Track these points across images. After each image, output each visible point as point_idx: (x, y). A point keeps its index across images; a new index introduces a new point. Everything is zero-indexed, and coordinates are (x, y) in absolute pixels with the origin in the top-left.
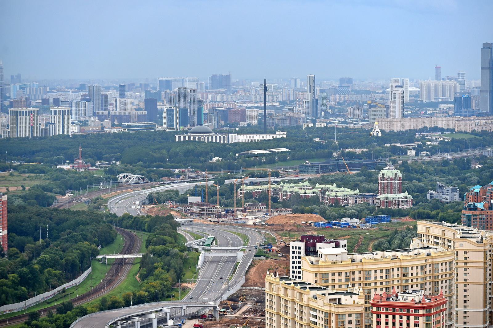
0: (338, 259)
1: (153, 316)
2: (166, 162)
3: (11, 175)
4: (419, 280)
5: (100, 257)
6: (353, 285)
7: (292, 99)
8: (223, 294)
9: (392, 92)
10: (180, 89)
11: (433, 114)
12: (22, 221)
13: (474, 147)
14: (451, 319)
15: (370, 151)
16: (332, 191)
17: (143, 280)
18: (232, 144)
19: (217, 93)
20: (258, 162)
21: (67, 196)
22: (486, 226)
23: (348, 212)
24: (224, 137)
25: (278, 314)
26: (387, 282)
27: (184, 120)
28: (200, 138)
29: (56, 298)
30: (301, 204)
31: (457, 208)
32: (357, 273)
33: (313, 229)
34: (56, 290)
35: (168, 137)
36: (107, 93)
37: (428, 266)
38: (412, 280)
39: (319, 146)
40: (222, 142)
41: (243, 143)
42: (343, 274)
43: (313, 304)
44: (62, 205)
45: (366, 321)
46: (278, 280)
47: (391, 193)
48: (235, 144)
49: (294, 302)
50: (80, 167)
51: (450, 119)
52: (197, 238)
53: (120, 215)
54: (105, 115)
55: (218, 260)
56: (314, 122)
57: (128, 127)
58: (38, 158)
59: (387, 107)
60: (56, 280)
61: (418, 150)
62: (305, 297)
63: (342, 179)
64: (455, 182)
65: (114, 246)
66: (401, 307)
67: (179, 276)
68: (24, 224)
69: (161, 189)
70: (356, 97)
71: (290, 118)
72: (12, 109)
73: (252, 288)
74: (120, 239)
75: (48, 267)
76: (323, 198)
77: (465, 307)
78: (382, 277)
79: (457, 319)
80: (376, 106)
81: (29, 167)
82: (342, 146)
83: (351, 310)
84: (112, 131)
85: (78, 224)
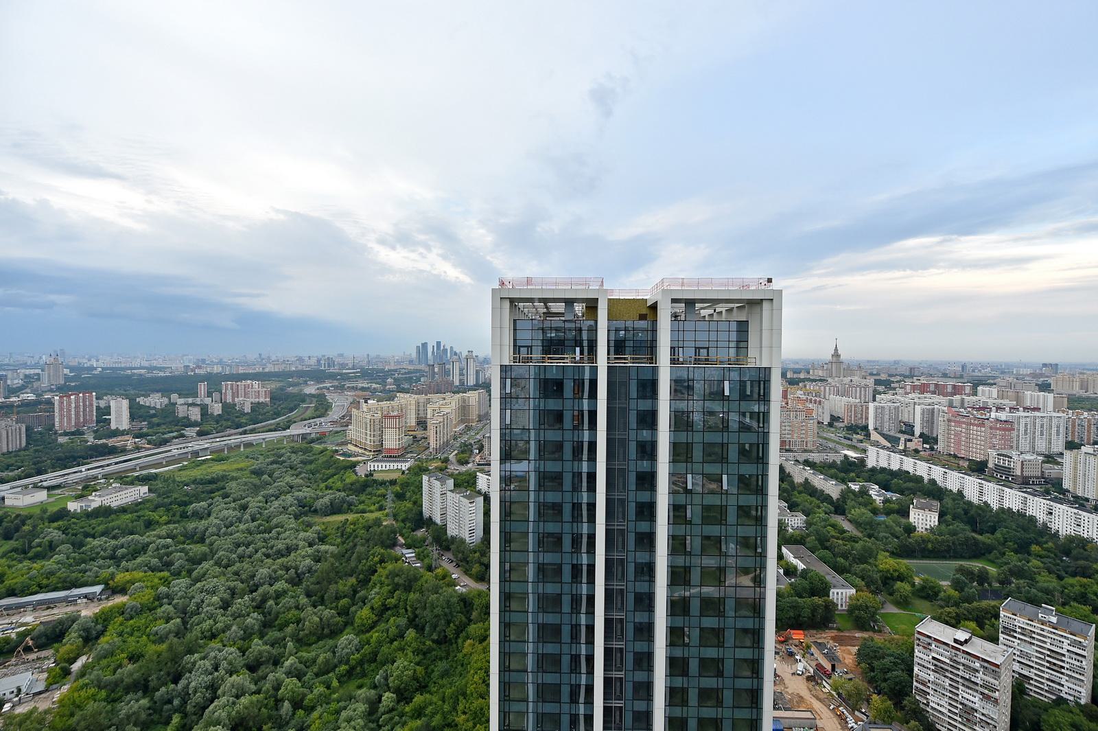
20: (352, 377)
30: (363, 389)
67: (326, 410)
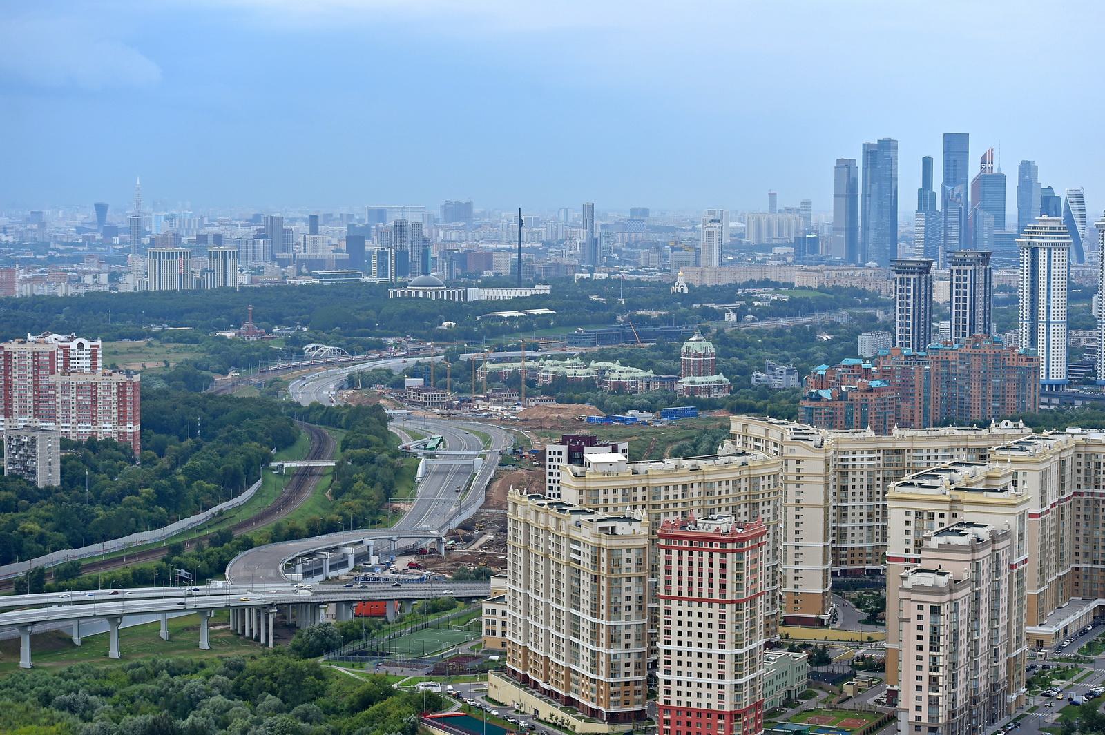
0: (613, 469)
1: (349, 551)
2: (374, 327)
3: (149, 344)
4: (731, 501)
5: (274, 464)
6: (635, 507)
7: (560, 237)
8: (451, 519)
9: (704, 228)
10: (397, 222)
11: (764, 261)
12: (162, 413)
13: (822, 309)
14: (775, 557)
15: (670, 315)
16: (614, 371)
17: (336, 498)
18: (470, 302)
19: (451, 228)
20: (509, 328)
21: (229, 376)
22: (834, 424)
23: (636, 402)
24: (459, 292)
25: (525, 548)
26: (684, 504)
27: (402, 268)
28: (425, 293)
29: (208, 524)
31: (793, 396)
32: (640, 490)
33: (585, 427)
34: (209, 513)
35: (378, 291)
36: (293, 228)
37: (743, 480)
38: (720, 501)
39: (597, 306)
40: (457, 299)
41: (486, 301)
42: (620, 492)
43: (575, 534)
44: (222, 390)
45: (653, 559)
46: (526, 500)
47: (699, 375)
48: (476, 303)
49: (548, 531)
50: (249, 334)
51: (787, 268)
52: (416, 438)
53: (306, 403)
54: (289, 259)
55: (446, 469)
56: (591, 271)
57: (321, 276)
58: (188, 321)
59: (698, 251)
60: (209, 498)
61: (741, 314)
62: (563, 524)
63: (629, 355)
64: (792, 359)
65: (296, 448)
66: (701, 539)
67: (388, 492)
68: (166, 416)
69: (366, 367)
70: (654, 237)
71: (558, 265)
72: (153, 250)
73: (494, 511)
74: (305, 438)
75: (198, 479)
76: (601, 382)
77: (797, 540)
78: (676, 496)
79: (785, 558)
80: (681, 249)
81: (175, 334)
82: (632, 306)
83: (631, 543)
84: (298, 282)
85: (243, 416)
